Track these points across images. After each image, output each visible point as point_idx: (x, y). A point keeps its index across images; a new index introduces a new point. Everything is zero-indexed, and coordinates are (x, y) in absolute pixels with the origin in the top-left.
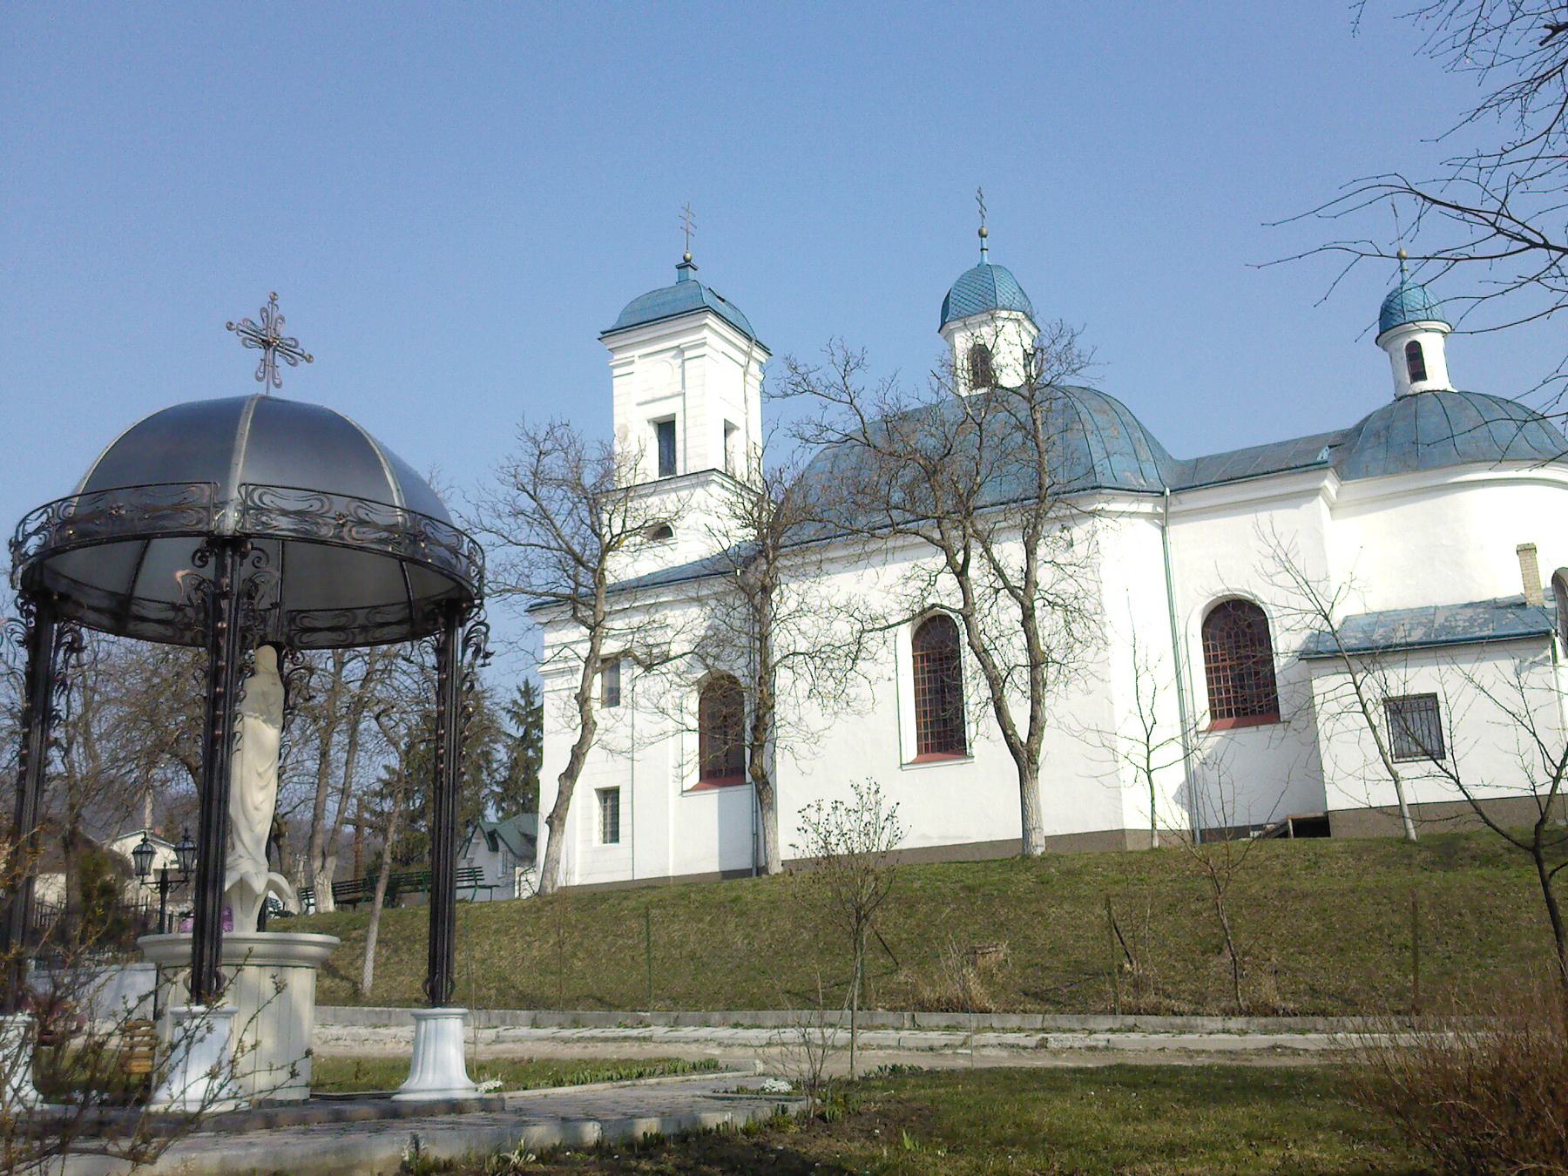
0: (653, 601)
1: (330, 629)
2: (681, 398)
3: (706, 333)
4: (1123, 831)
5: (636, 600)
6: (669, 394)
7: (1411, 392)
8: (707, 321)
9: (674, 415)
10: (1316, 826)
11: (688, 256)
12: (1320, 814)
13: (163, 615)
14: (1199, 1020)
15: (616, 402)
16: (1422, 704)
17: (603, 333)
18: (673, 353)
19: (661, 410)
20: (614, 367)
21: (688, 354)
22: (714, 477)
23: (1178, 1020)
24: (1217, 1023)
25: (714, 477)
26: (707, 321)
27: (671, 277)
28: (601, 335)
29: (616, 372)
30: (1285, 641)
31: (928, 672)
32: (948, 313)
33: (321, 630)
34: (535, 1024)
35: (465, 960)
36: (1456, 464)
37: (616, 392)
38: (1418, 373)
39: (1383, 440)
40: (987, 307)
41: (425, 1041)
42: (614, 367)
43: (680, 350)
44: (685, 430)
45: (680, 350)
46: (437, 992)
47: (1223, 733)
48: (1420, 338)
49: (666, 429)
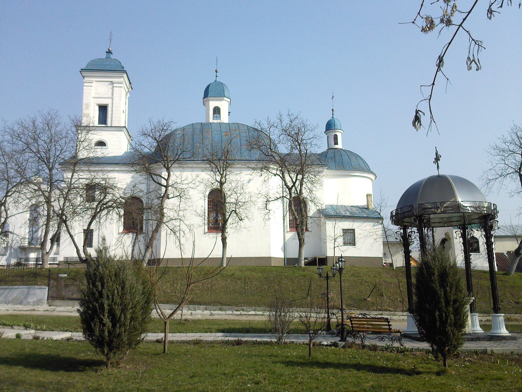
0: (113, 169)
1: (457, 221)
2: (111, 99)
3: (122, 79)
4: (270, 257)
5: (115, 168)
6: (106, 97)
7: (334, 148)
8: (124, 76)
9: (108, 104)
10: (323, 261)
11: (110, 49)
12: (325, 257)
13: (457, 219)
14: (397, 313)
15: (84, 95)
16: (350, 232)
17: (81, 69)
18: (109, 83)
19: (103, 102)
20: (84, 82)
21: (115, 85)
22: (124, 129)
23: (392, 313)
24: (401, 313)
25: (124, 129)
26: (124, 76)
27: (104, 56)
28: (81, 70)
29: (85, 84)
30: (312, 210)
31: (212, 205)
32: (206, 94)
33: (454, 221)
34: (221, 310)
35: (501, 305)
36: (353, 171)
37: (84, 91)
38: (336, 143)
39: (333, 160)
40: (221, 94)
41: (499, 323)
42: (84, 82)
43: (112, 83)
44: (112, 110)
45: (112, 83)
46: (496, 310)
47: (294, 232)
48: (337, 133)
49: (103, 109)
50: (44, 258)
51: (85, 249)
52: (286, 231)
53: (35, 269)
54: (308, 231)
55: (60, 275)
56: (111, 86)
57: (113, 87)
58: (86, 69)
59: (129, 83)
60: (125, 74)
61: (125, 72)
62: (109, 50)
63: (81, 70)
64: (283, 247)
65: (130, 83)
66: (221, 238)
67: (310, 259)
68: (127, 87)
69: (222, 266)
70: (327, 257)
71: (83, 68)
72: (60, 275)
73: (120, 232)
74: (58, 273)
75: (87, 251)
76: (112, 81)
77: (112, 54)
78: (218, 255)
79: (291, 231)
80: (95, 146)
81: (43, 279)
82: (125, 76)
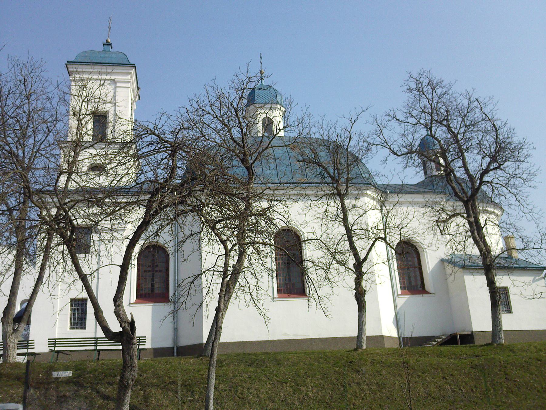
11: (109, 40)
12: (470, 333)
17: (68, 62)
21: (118, 85)
26: (132, 71)
28: (67, 63)
50: (8, 341)
51: (119, 306)
52: (396, 294)
53: (214, 151)
54: (428, 293)
55: (55, 374)
56: (113, 86)
57: (116, 88)
58: (76, 61)
59: (136, 88)
60: (134, 70)
61: (133, 66)
62: (107, 41)
63: (67, 63)
64: (395, 319)
65: (138, 88)
66: (355, 291)
67: (444, 337)
68: (134, 95)
69: (361, 348)
70: (472, 332)
71: (72, 60)
72: (55, 374)
73: (131, 302)
74: (52, 368)
75: (124, 311)
76: (114, 80)
77: (111, 48)
78: (297, 335)
79: (402, 294)
80: (88, 170)
81: (6, 386)
82: (133, 71)
